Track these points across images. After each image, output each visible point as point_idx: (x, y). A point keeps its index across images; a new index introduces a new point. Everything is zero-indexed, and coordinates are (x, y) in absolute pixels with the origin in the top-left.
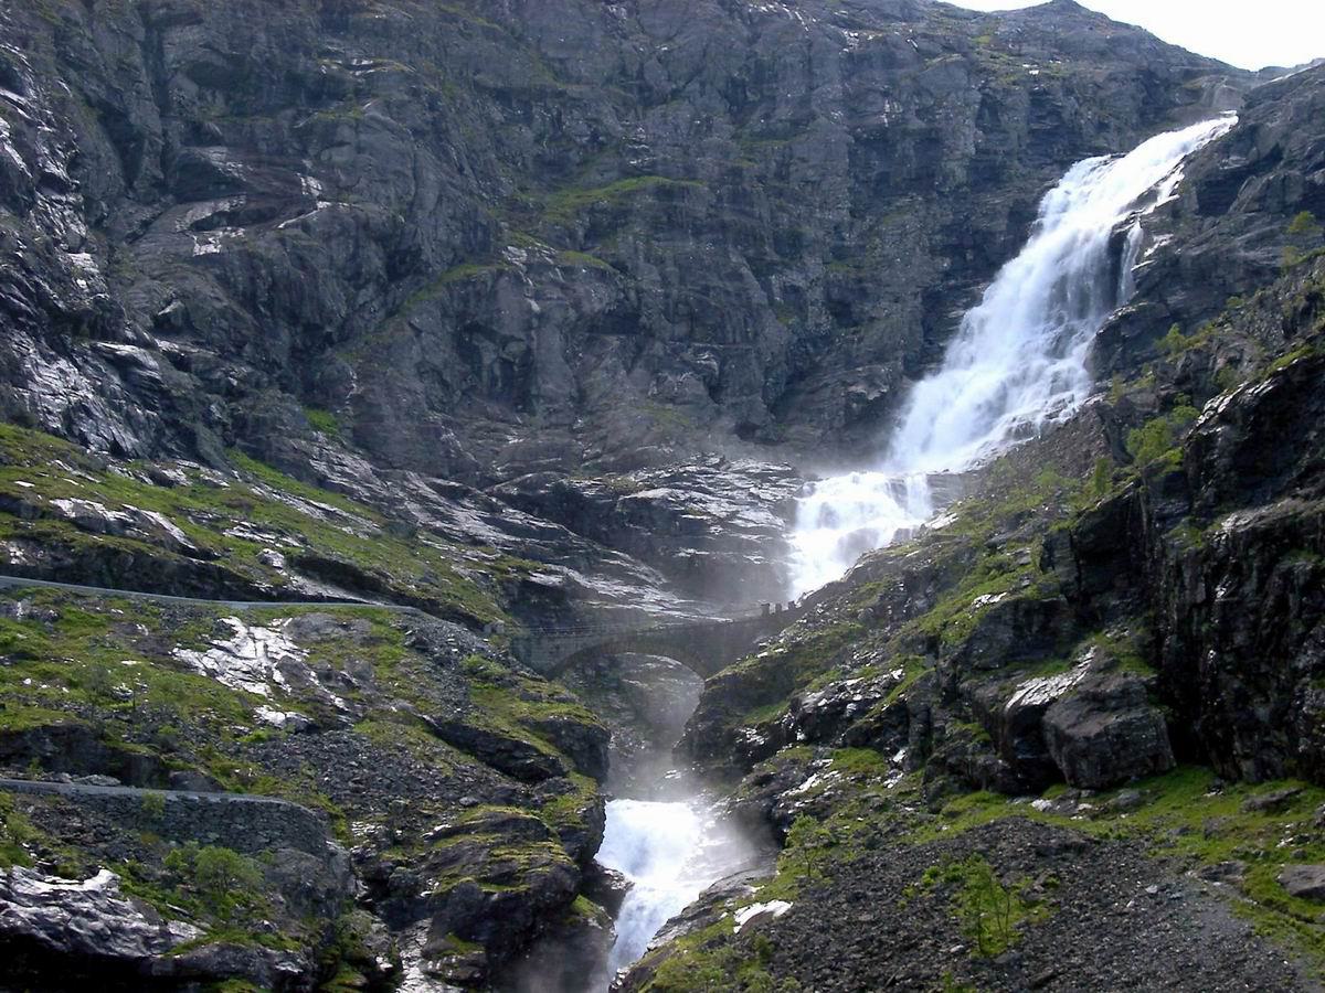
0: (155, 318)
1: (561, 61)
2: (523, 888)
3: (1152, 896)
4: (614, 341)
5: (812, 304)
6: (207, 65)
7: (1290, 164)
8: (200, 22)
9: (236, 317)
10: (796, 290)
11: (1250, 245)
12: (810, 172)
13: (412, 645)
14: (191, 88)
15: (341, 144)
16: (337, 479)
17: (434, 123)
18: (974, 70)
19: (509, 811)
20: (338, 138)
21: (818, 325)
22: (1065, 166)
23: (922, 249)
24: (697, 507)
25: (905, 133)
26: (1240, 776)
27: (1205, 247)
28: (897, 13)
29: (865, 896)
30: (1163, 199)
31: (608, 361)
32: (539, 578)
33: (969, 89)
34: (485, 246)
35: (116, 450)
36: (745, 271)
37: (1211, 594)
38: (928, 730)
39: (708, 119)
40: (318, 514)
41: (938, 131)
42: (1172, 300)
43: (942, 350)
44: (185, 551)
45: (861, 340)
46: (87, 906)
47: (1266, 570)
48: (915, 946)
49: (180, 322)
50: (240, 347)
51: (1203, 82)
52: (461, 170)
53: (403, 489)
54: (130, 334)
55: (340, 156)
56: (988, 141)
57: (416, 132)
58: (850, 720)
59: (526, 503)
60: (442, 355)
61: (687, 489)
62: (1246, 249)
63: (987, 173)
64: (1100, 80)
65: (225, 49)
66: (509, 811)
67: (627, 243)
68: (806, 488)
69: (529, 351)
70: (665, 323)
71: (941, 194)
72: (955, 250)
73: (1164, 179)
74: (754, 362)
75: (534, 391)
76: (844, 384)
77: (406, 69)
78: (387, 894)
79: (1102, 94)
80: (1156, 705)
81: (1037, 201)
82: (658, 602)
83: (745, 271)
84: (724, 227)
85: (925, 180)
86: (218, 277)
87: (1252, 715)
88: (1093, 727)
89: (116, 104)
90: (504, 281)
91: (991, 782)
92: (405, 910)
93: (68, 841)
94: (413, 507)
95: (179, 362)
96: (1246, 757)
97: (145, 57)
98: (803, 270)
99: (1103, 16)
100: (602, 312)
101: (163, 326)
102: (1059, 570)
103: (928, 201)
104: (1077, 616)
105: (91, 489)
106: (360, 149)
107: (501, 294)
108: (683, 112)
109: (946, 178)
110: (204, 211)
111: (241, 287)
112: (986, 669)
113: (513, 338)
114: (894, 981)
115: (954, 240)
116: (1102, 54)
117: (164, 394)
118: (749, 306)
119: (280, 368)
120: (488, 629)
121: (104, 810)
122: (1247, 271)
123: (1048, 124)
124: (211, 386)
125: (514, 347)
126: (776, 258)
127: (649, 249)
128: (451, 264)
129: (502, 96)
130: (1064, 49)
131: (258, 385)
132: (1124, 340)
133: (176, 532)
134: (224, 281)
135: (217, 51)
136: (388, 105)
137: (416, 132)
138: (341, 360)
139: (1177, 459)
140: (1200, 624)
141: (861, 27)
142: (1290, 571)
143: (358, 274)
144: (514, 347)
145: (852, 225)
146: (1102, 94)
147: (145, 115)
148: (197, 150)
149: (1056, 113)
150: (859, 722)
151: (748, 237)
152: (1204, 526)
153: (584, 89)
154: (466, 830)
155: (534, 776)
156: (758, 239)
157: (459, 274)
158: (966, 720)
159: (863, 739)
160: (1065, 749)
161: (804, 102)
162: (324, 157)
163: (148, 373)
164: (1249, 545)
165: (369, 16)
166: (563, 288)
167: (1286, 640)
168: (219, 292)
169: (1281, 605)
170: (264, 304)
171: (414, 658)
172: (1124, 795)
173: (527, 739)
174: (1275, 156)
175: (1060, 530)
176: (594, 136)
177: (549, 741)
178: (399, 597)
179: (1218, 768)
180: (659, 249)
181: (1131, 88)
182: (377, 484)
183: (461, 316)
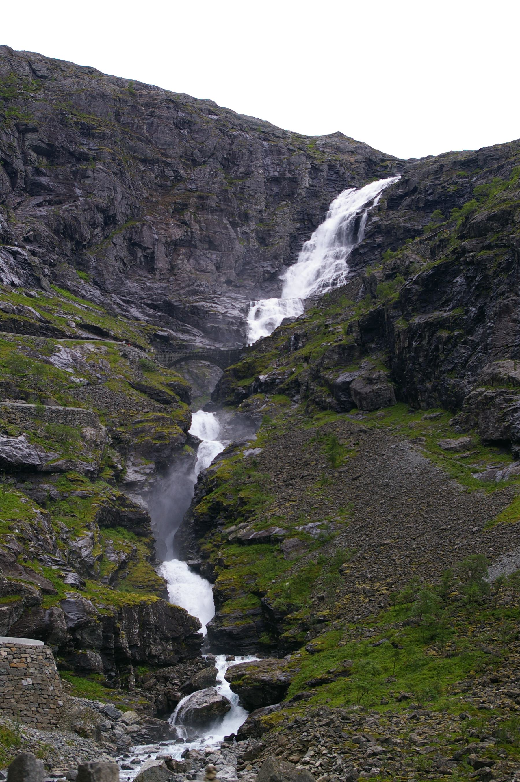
0: (24, 237)
2: (167, 442)
3: (393, 449)
6: (40, 147)
7: (420, 193)
8: (38, 131)
9: (53, 238)
10: (246, 233)
11: (405, 221)
12: (251, 192)
13: (122, 356)
14: (34, 155)
15: (89, 177)
16: (88, 296)
17: (120, 170)
18: (308, 157)
19: (160, 414)
20: (87, 175)
22: (340, 192)
23: (290, 220)
24: (214, 309)
25: (285, 179)
26: (420, 407)
27: (390, 222)
28: (281, 136)
29: (289, 447)
30: (375, 204)
31: (181, 257)
32: (160, 333)
33: (306, 164)
34: (138, 215)
35: (13, 284)
36: (229, 226)
37: (410, 344)
38: (308, 388)
39: (215, 172)
40: (83, 309)
41: (296, 178)
42: (378, 240)
43: (297, 256)
44: (41, 321)
46: (20, 446)
47: (432, 335)
48: (309, 464)
49: (32, 239)
50: (54, 248)
51: (388, 163)
52: (130, 187)
53: (111, 300)
54: (16, 243)
55: (88, 182)
57: (114, 173)
58: (277, 385)
59: (153, 307)
60: (123, 253)
61: (210, 303)
63: (313, 193)
64: (352, 161)
65: (46, 141)
66: (160, 414)
67: (187, 216)
68: (251, 303)
69: (154, 252)
72: (302, 221)
73: (376, 197)
75: (155, 267)
76: (263, 267)
77: (111, 151)
78: (119, 443)
79: (353, 166)
80: (389, 382)
81: (329, 204)
82: (201, 342)
83: (229, 226)
84: (222, 210)
85: (291, 195)
86: (46, 223)
88: (368, 389)
89: (8, 160)
91: (331, 408)
92: (126, 449)
93: (11, 423)
94: (114, 307)
95: (33, 253)
96: (423, 401)
97: (19, 143)
98: (248, 226)
99: (352, 139)
100: (179, 239)
101: (27, 240)
102: (354, 334)
103: (292, 203)
105: (6, 298)
106: (95, 179)
108: (207, 169)
109: (298, 194)
110: (40, 199)
112: (328, 368)
113: (148, 248)
114: (303, 477)
115: (301, 217)
116: (352, 152)
117: (29, 264)
118: (230, 238)
119: (68, 256)
120: (147, 351)
121: (22, 412)
123: (334, 177)
124: (45, 262)
125: (148, 251)
128: (126, 221)
129: (143, 161)
130: (339, 150)
131: (60, 262)
132: (361, 253)
133: (37, 314)
134: (48, 225)
135: (43, 142)
136: (104, 163)
137: (114, 173)
138: (89, 255)
139: (397, 296)
140: (406, 354)
141: (269, 140)
142: (440, 336)
143: (94, 224)
144: (148, 251)
145: (265, 211)
147: (18, 164)
148: (37, 178)
149: (337, 173)
150: (281, 386)
151: (231, 214)
152: (408, 320)
153: (173, 160)
154: (147, 421)
155: (167, 402)
156: (232, 214)
157: (129, 225)
158: (322, 386)
159: (282, 392)
160: (358, 397)
164: (425, 328)
165: (95, 131)
166: (165, 230)
167: (438, 361)
168: (46, 229)
169: (437, 349)
170: (62, 233)
171: (123, 360)
172: (379, 413)
173: (164, 389)
174: (415, 190)
175: (355, 321)
176: (176, 177)
177: (172, 390)
178: (115, 338)
179: (412, 405)
180: (199, 217)
181: (363, 165)
182: (102, 298)
183: (130, 239)
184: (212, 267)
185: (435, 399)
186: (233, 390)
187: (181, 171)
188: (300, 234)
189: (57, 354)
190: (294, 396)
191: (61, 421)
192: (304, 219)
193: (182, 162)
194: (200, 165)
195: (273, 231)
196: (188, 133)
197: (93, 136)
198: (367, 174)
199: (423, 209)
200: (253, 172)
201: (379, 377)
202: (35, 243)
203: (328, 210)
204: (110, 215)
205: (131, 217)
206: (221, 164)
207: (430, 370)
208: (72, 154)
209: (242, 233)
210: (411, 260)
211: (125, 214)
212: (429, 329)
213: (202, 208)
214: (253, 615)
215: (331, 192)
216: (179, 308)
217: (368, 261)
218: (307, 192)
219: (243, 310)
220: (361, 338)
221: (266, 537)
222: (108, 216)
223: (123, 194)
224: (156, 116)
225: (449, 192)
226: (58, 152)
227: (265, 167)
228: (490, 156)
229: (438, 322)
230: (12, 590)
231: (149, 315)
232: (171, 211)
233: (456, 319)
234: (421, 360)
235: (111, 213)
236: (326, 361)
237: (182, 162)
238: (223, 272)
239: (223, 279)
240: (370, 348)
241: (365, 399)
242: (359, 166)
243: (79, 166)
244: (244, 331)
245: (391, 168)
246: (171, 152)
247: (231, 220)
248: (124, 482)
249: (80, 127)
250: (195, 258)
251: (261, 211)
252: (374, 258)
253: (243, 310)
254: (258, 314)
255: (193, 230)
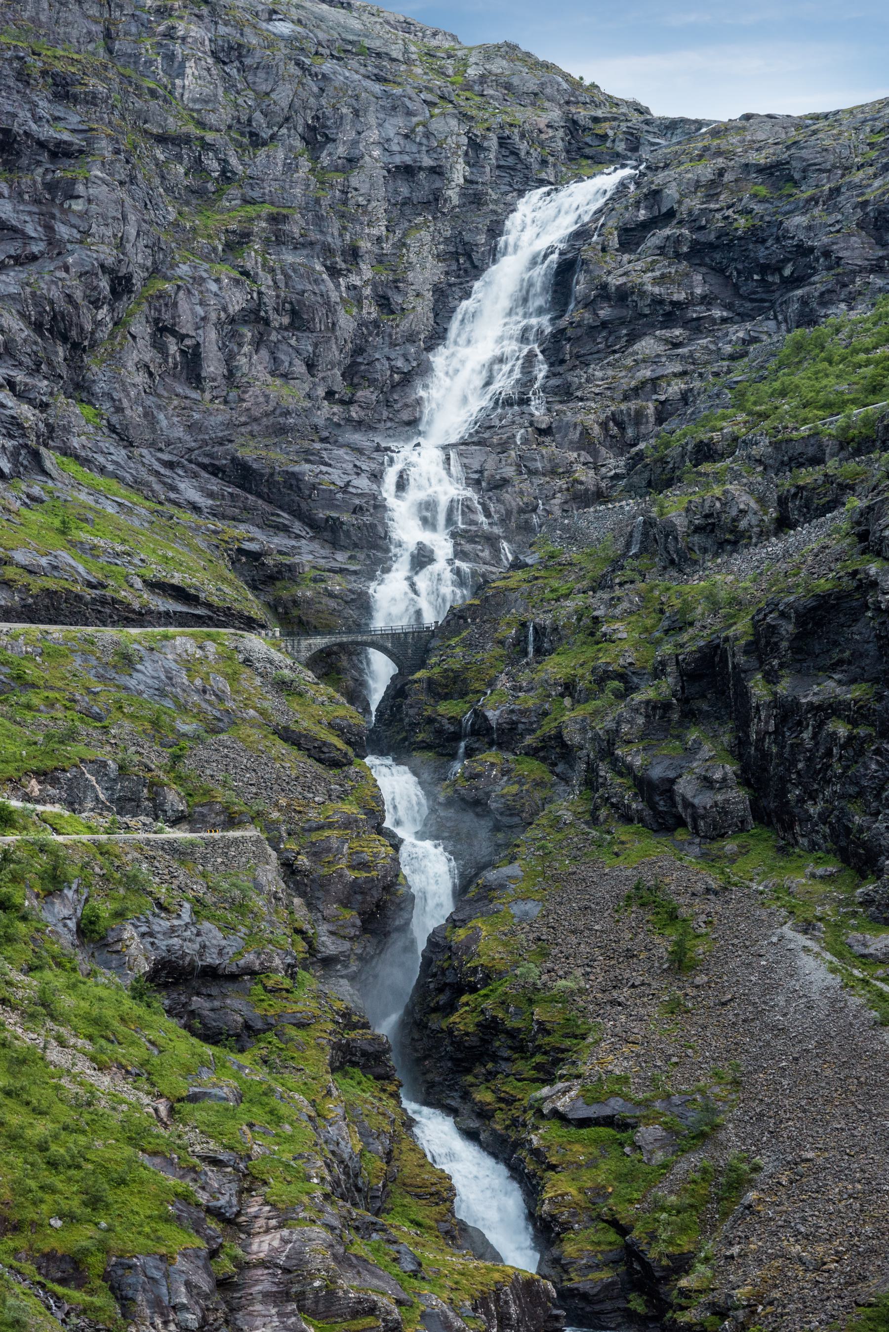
1: (199, 111)
4: (248, 333)
5: (366, 298)
10: (355, 287)
15: (78, 197)
20: (76, 193)
21: (369, 313)
22: (521, 193)
24: (326, 477)
33: (458, 135)
36: (325, 276)
45: (397, 326)
50: (38, 365)
55: (78, 206)
56: (472, 173)
59: (215, 470)
60: (148, 355)
62: (653, 285)
64: (542, 126)
67: (251, 259)
69: (198, 344)
70: (276, 316)
71: (443, 213)
72: (455, 255)
74: (334, 346)
75: (203, 374)
79: (543, 136)
87: (807, 811)
90: (181, 294)
92: (306, 885)
96: (803, 836)
98: (359, 272)
104: (682, 711)
107: (180, 302)
109: (445, 200)
111: (33, 319)
112: (629, 742)
113: (188, 336)
122: (653, 300)
123: (511, 161)
125: (188, 342)
126: (344, 266)
127: (265, 260)
129: (162, 139)
134: (23, 315)
144: (188, 342)
145: (387, 238)
146: (543, 136)
149: (515, 153)
155: (335, 764)
161: (355, 143)
162: (66, 206)
163: (8, 412)
164: (808, 712)
167: (829, 773)
176: (223, 172)
177: (338, 736)
179: (781, 834)
181: (561, 133)
183: (157, 321)
184: (300, 368)
185: (824, 837)
186: (430, 721)
187: (234, 161)
188: (450, 285)
189: (139, 667)
190: (556, 765)
191: (219, 860)
192: (457, 253)
193: (233, 139)
194: (264, 144)
195: (404, 281)
196: (239, 70)
197: (75, 99)
198: (568, 152)
199: (687, 257)
200: (362, 157)
201: (724, 779)
202: (7, 358)
203: (500, 234)
204: (120, 274)
205: (155, 272)
206: (303, 138)
207: (816, 786)
208: (42, 144)
209: (348, 288)
210: (742, 506)
211: (143, 267)
212: (815, 715)
213: (279, 239)
214: (613, 1262)
215: (506, 193)
216: (262, 475)
217: (584, 355)
218: (462, 195)
219: (375, 476)
220: (683, 688)
221: (608, 1117)
222: (117, 277)
223: (139, 226)
224: (178, 38)
225: (736, 229)
226: (19, 143)
227: (384, 144)
228: (815, 164)
229: (830, 705)
230: (363, 1309)
231: (211, 495)
232: (220, 248)
233: (861, 707)
234: (800, 766)
235: (123, 271)
236: (625, 728)
237: (233, 139)
238: (321, 375)
239: (321, 392)
240: (700, 711)
241: (703, 817)
242: (554, 137)
243: (59, 174)
244: (385, 526)
245: (614, 141)
246: (212, 119)
247: (328, 263)
248: (319, 956)
249: (50, 80)
250: (267, 347)
251: (379, 240)
252: (595, 349)
253: (375, 476)
254: (401, 485)
255: (263, 289)
